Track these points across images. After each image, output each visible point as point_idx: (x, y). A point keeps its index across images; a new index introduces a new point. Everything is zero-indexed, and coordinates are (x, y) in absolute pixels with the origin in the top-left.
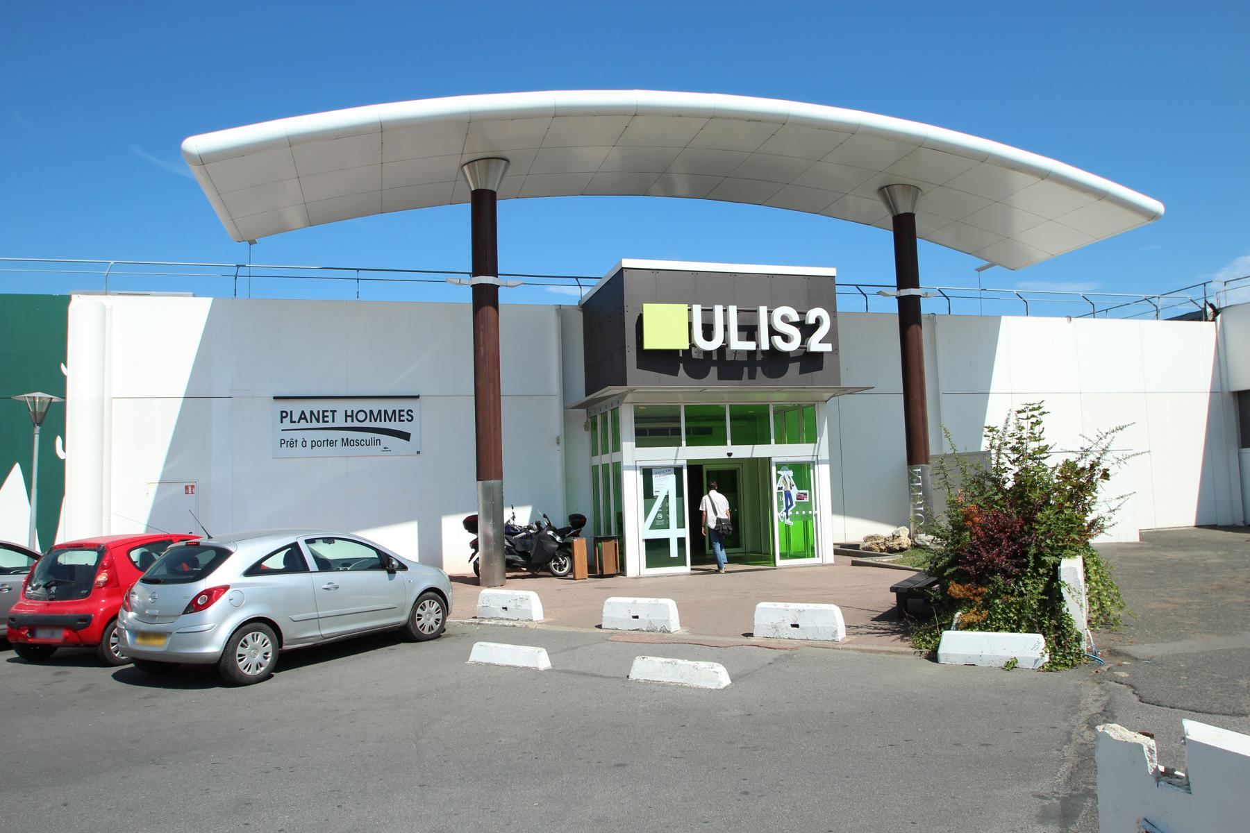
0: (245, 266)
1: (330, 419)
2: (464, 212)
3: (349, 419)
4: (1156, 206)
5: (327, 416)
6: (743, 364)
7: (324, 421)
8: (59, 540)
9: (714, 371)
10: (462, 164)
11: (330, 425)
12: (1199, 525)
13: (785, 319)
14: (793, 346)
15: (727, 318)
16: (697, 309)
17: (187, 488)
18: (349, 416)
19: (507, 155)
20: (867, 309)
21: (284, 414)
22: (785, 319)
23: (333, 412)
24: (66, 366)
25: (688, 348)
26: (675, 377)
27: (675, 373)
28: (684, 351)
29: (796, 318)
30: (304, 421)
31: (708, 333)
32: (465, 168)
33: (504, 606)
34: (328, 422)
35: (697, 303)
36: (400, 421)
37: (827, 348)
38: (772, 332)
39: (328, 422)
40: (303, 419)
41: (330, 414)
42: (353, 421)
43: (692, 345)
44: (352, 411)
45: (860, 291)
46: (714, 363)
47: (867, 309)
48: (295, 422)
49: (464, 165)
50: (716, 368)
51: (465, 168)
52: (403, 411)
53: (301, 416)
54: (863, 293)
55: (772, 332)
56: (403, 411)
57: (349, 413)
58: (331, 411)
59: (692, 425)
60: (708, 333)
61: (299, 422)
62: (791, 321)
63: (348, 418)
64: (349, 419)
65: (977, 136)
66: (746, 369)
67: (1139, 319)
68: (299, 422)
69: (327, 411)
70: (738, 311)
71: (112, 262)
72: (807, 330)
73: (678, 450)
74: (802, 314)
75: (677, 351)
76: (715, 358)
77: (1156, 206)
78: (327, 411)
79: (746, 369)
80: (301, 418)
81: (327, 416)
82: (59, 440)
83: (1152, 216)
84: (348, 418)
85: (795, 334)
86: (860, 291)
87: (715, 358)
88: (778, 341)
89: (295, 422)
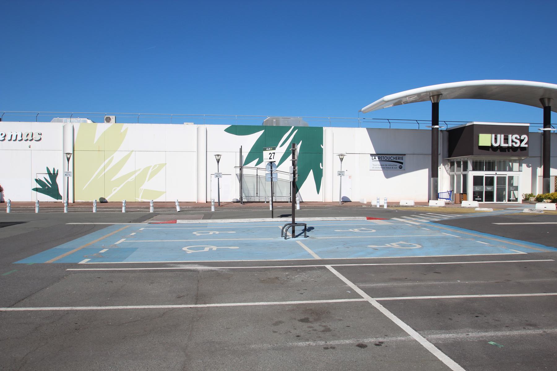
1: (382, 159)
9: (499, 150)
12: (429, 160)
13: (516, 138)
14: (517, 145)
15: (501, 137)
16: (493, 135)
17: (349, 177)
21: (379, 157)
22: (516, 138)
23: (383, 157)
24: (323, 146)
26: (525, 151)
29: (519, 138)
31: (496, 142)
32: (431, 97)
37: (526, 146)
38: (513, 141)
41: (383, 158)
43: (492, 144)
46: (499, 148)
51: (431, 97)
55: (513, 141)
57: (394, 158)
59: (98, 210)
60: (496, 142)
66: (507, 150)
67: (94, 231)
70: (504, 136)
72: (521, 141)
73: (430, 154)
74: (520, 137)
79: (507, 150)
82: (321, 164)
85: (518, 142)
88: (514, 144)
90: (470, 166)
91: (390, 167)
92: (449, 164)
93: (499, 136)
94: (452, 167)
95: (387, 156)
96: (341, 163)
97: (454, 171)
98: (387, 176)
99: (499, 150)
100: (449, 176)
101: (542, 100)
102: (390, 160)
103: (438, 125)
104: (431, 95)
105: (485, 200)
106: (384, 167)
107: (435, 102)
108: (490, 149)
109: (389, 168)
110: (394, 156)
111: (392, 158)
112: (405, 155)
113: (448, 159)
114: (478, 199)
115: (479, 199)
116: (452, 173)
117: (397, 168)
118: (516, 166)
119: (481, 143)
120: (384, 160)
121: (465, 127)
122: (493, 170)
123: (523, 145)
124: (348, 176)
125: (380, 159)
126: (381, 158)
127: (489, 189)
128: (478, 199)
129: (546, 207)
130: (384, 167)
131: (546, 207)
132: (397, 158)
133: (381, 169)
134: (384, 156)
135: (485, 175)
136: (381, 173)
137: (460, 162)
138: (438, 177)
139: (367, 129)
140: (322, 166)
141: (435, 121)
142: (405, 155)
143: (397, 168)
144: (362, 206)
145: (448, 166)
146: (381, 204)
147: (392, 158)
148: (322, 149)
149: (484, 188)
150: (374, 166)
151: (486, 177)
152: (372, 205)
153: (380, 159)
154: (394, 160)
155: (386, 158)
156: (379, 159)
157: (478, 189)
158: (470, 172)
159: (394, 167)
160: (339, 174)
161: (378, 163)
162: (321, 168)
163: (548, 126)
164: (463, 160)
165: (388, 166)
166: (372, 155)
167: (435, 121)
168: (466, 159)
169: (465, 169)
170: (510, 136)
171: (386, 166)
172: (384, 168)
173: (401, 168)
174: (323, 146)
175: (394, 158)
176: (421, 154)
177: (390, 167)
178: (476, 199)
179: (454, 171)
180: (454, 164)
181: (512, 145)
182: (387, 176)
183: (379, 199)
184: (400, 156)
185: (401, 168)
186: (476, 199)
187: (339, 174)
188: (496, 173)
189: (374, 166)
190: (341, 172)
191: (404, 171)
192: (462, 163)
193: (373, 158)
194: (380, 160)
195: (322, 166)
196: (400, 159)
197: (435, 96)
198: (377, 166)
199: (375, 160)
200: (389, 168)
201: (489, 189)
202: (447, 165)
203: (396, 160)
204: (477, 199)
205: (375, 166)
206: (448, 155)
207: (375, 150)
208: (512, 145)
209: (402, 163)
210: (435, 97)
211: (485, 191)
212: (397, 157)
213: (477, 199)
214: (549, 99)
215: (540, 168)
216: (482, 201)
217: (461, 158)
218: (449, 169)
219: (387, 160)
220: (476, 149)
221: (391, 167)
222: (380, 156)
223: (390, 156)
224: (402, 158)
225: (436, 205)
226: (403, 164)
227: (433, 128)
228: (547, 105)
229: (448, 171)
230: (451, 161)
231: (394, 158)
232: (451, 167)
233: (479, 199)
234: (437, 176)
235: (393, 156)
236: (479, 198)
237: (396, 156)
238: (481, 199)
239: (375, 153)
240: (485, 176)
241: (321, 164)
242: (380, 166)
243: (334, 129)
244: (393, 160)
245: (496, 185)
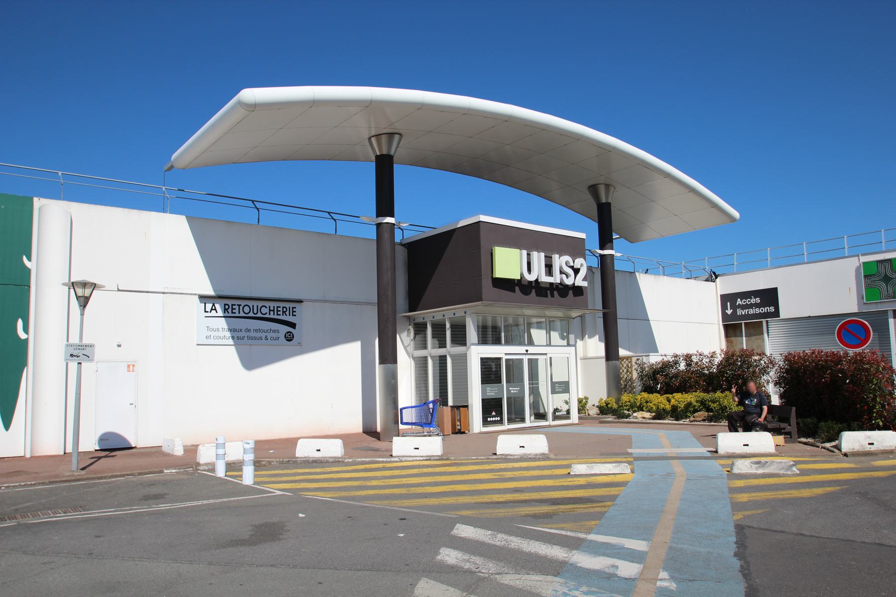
0: (183, 191)
1: (237, 311)
2: (370, 170)
3: (272, 312)
4: (736, 214)
5: (235, 309)
6: (546, 289)
7: (277, 315)
8: (846, 327)
9: (534, 291)
10: (371, 136)
11: (237, 315)
15: (539, 259)
16: (525, 252)
17: (129, 366)
18: (272, 311)
19: (401, 132)
20: (336, 232)
21: (227, 307)
23: (239, 305)
24: (29, 259)
25: (520, 278)
26: (582, 296)
27: (514, 291)
28: (518, 280)
30: (215, 311)
33: (318, 449)
34: (235, 313)
35: (538, 250)
36: (293, 315)
37: (585, 284)
39: (235, 313)
40: (213, 310)
41: (237, 307)
42: (274, 315)
43: (522, 275)
44: (274, 307)
45: (255, 205)
46: (534, 288)
47: (336, 232)
48: (208, 312)
49: (372, 137)
50: (571, 291)
52: (280, 307)
53: (212, 307)
54: (256, 208)
55: (562, 272)
56: (280, 307)
57: (272, 309)
58: (238, 305)
61: (210, 312)
62: (569, 265)
63: (271, 312)
64: (272, 312)
65: (663, 161)
66: (549, 292)
68: (210, 312)
69: (235, 305)
70: (545, 257)
71: (60, 173)
75: (514, 280)
76: (534, 285)
77: (736, 214)
78: (235, 305)
79: (549, 292)
80: (212, 309)
81: (235, 309)
82: (20, 323)
83: (732, 219)
84: (271, 312)
86: (255, 205)
87: (534, 285)
89: (208, 312)
90: (472, 334)
91: (258, 335)
92: (412, 330)
93: (535, 254)
94: (416, 337)
95: (250, 303)
96: (82, 315)
97: (425, 347)
98: (250, 363)
99: (534, 291)
100: (413, 362)
101: (593, 189)
102: (259, 315)
103: (392, 216)
104: (373, 133)
105: (508, 420)
106: (241, 334)
107: (385, 152)
108: (517, 288)
109: (255, 338)
110: (272, 305)
111: (264, 310)
112: (301, 301)
113: (409, 318)
114: (494, 419)
115: (496, 419)
116: (422, 353)
117: (278, 339)
118: (538, 335)
119: (501, 272)
120: (242, 314)
121: (453, 231)
122: (497, 341)
123: (580, 282)
124: (125, 365)
125: (230, 310)
126: (232, 309)
127: (514, 390)
128: (494, 419)
129: (747, 445)
130: (241, 334)
131: (747, 445)
132: (278, 311)
133: (231, 342)
134: (243, 303)
135: (506, 354)
136: (230, 354)
137: (424, 326)
138: (397, 363)
139: (190, 219)
140: (26, 329)
141: (385, 205)
142: (301, 301)
143: (278, 339)
144: (162, 472)
145: (408, 335)
146: (231, 458)
147: (264, 310)
148: (28, 271)
149: (504, 390)
150: (209, 333)
151: (507, 360)
152: (198, 464)
153: (230, 310)
154: (272, 316)
155: (247, 309)
156: (225, 310)
157: (492, 392)
158: (472, 346)
159: (269, 335)
160: (72, 355)
161: (222, 323)
162: (22, 335)
163: (609, 245)
164: (432, 319)
165: (252, 334)
166: (203, 298)
167: (385, 205)
168: (460, 313)
169: (460, 338)
170: (556, 257)
171: (248, 334)
172: (238, 336)
173: (289, 338)
174: (29, 259)
175: (272, 309)
176: (342, 302)
177: (258, 335)
178: (489, 419)
179: (425, 347)
180: (427, 328)
181: (562, 280)
182: (250, 363)
183: (223, 445)
184: (287, 305)
185: (289, 338)
186: (489, 419)
187: (72, 355)
188: (527, 351)
189: (209, 333)
190: (81, 347)
191: (612, 189)
192: (448, 326)
193: (208, 309)
194: (229, 313)
195: (26, 329)
196: (287, 313)
197: (383, 135)
198: (221, 334)
199: (213, 313)
200: (255, 338)
201: (514, 390)
202: (405, 333)
203: (276, 317)
204: (491, 419)
205: (213, 334)
206: (407, 307)
207: (212, 286)
208: (562, 280)
209: (293, 325)
210: (384, 139)
211: (507, 398)
212: (277, 307)
213: (491, 419)
214: (607, 186)
215: (582, 340)
216: (501, 422)
217: (446, 314)
218: (412, 343)
219: (251, 314)
220: (487, 284)
221: (263, 335)
222: (230, 302)
223: (260, 304)
224: (293, 312)
225: (417, 453)
226: (295, 328)
227: (379, 225)
228: (604, 201)
229: (408, 348)
230: (416, 321)
231: (270, 310)
232: (415, 337)
233: (496, 419)
234: (394, 361)
235: (267, 304)
236: (494, 416)
237: (276, 304)
238: (499, 419)
239: (211, 292)
240: (505, 357)
241: (20, 323)
242: (228, 334)
243: (79, 210)
244: (267, 316)
245: (528, 382)
